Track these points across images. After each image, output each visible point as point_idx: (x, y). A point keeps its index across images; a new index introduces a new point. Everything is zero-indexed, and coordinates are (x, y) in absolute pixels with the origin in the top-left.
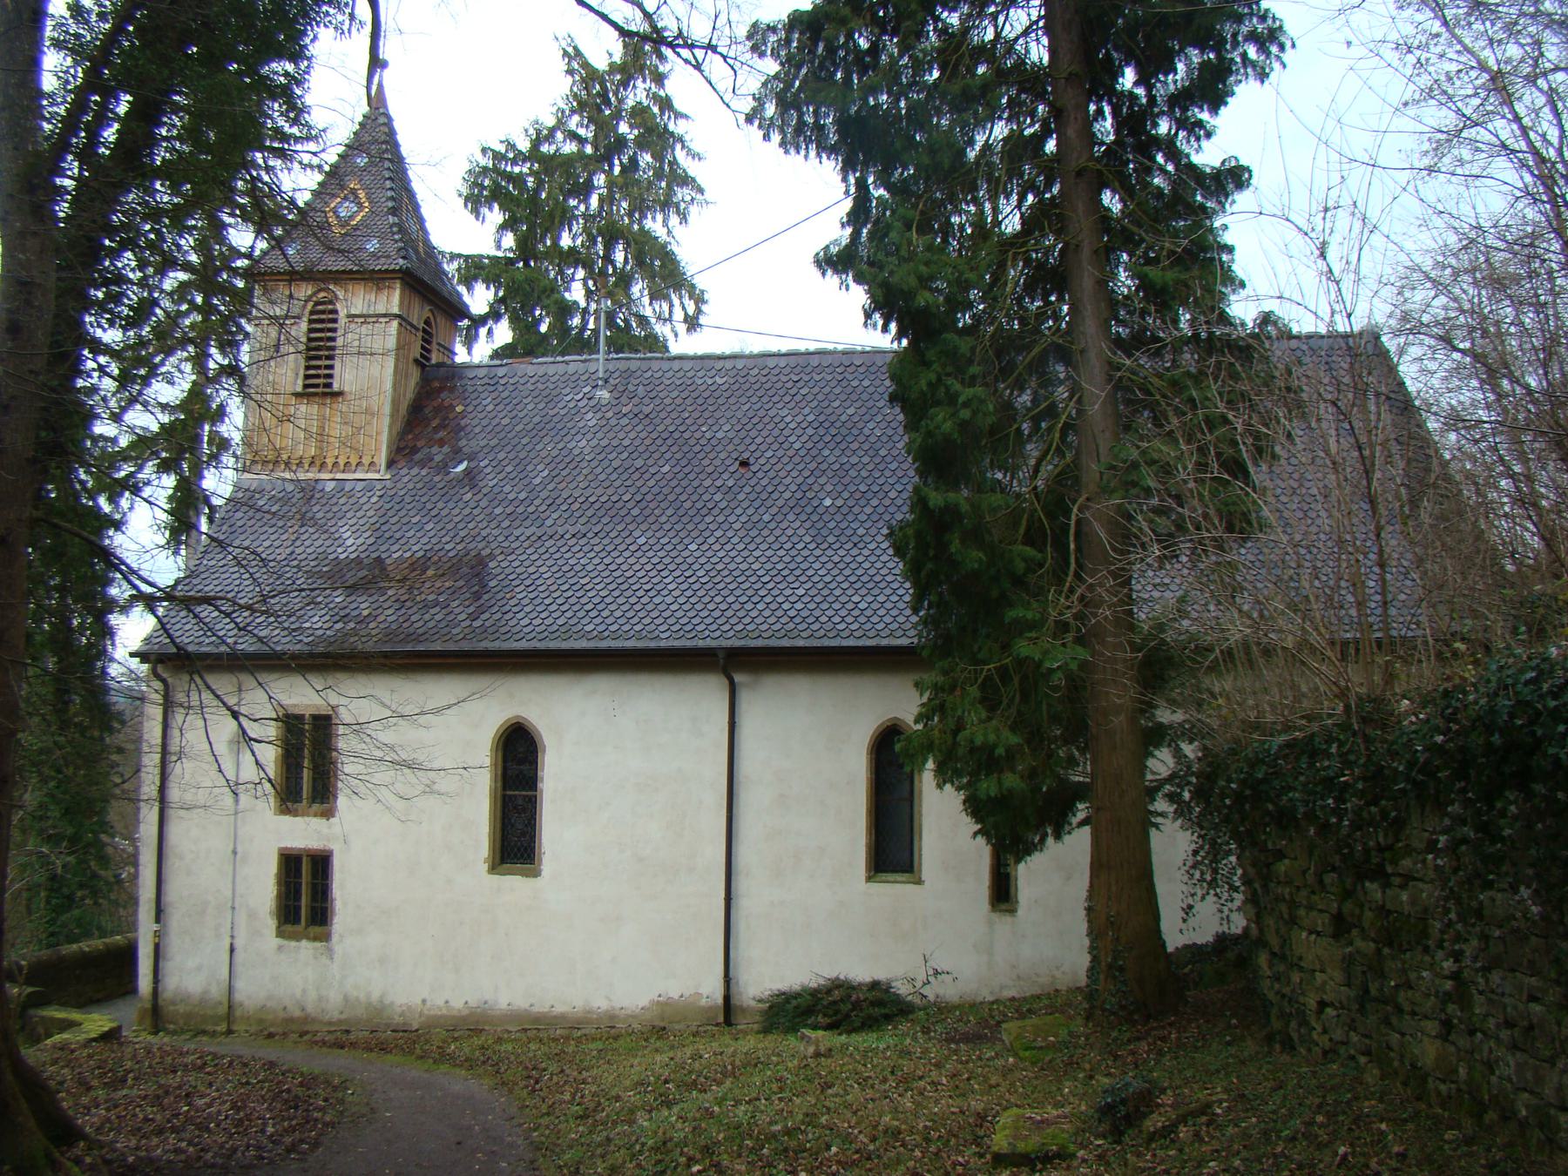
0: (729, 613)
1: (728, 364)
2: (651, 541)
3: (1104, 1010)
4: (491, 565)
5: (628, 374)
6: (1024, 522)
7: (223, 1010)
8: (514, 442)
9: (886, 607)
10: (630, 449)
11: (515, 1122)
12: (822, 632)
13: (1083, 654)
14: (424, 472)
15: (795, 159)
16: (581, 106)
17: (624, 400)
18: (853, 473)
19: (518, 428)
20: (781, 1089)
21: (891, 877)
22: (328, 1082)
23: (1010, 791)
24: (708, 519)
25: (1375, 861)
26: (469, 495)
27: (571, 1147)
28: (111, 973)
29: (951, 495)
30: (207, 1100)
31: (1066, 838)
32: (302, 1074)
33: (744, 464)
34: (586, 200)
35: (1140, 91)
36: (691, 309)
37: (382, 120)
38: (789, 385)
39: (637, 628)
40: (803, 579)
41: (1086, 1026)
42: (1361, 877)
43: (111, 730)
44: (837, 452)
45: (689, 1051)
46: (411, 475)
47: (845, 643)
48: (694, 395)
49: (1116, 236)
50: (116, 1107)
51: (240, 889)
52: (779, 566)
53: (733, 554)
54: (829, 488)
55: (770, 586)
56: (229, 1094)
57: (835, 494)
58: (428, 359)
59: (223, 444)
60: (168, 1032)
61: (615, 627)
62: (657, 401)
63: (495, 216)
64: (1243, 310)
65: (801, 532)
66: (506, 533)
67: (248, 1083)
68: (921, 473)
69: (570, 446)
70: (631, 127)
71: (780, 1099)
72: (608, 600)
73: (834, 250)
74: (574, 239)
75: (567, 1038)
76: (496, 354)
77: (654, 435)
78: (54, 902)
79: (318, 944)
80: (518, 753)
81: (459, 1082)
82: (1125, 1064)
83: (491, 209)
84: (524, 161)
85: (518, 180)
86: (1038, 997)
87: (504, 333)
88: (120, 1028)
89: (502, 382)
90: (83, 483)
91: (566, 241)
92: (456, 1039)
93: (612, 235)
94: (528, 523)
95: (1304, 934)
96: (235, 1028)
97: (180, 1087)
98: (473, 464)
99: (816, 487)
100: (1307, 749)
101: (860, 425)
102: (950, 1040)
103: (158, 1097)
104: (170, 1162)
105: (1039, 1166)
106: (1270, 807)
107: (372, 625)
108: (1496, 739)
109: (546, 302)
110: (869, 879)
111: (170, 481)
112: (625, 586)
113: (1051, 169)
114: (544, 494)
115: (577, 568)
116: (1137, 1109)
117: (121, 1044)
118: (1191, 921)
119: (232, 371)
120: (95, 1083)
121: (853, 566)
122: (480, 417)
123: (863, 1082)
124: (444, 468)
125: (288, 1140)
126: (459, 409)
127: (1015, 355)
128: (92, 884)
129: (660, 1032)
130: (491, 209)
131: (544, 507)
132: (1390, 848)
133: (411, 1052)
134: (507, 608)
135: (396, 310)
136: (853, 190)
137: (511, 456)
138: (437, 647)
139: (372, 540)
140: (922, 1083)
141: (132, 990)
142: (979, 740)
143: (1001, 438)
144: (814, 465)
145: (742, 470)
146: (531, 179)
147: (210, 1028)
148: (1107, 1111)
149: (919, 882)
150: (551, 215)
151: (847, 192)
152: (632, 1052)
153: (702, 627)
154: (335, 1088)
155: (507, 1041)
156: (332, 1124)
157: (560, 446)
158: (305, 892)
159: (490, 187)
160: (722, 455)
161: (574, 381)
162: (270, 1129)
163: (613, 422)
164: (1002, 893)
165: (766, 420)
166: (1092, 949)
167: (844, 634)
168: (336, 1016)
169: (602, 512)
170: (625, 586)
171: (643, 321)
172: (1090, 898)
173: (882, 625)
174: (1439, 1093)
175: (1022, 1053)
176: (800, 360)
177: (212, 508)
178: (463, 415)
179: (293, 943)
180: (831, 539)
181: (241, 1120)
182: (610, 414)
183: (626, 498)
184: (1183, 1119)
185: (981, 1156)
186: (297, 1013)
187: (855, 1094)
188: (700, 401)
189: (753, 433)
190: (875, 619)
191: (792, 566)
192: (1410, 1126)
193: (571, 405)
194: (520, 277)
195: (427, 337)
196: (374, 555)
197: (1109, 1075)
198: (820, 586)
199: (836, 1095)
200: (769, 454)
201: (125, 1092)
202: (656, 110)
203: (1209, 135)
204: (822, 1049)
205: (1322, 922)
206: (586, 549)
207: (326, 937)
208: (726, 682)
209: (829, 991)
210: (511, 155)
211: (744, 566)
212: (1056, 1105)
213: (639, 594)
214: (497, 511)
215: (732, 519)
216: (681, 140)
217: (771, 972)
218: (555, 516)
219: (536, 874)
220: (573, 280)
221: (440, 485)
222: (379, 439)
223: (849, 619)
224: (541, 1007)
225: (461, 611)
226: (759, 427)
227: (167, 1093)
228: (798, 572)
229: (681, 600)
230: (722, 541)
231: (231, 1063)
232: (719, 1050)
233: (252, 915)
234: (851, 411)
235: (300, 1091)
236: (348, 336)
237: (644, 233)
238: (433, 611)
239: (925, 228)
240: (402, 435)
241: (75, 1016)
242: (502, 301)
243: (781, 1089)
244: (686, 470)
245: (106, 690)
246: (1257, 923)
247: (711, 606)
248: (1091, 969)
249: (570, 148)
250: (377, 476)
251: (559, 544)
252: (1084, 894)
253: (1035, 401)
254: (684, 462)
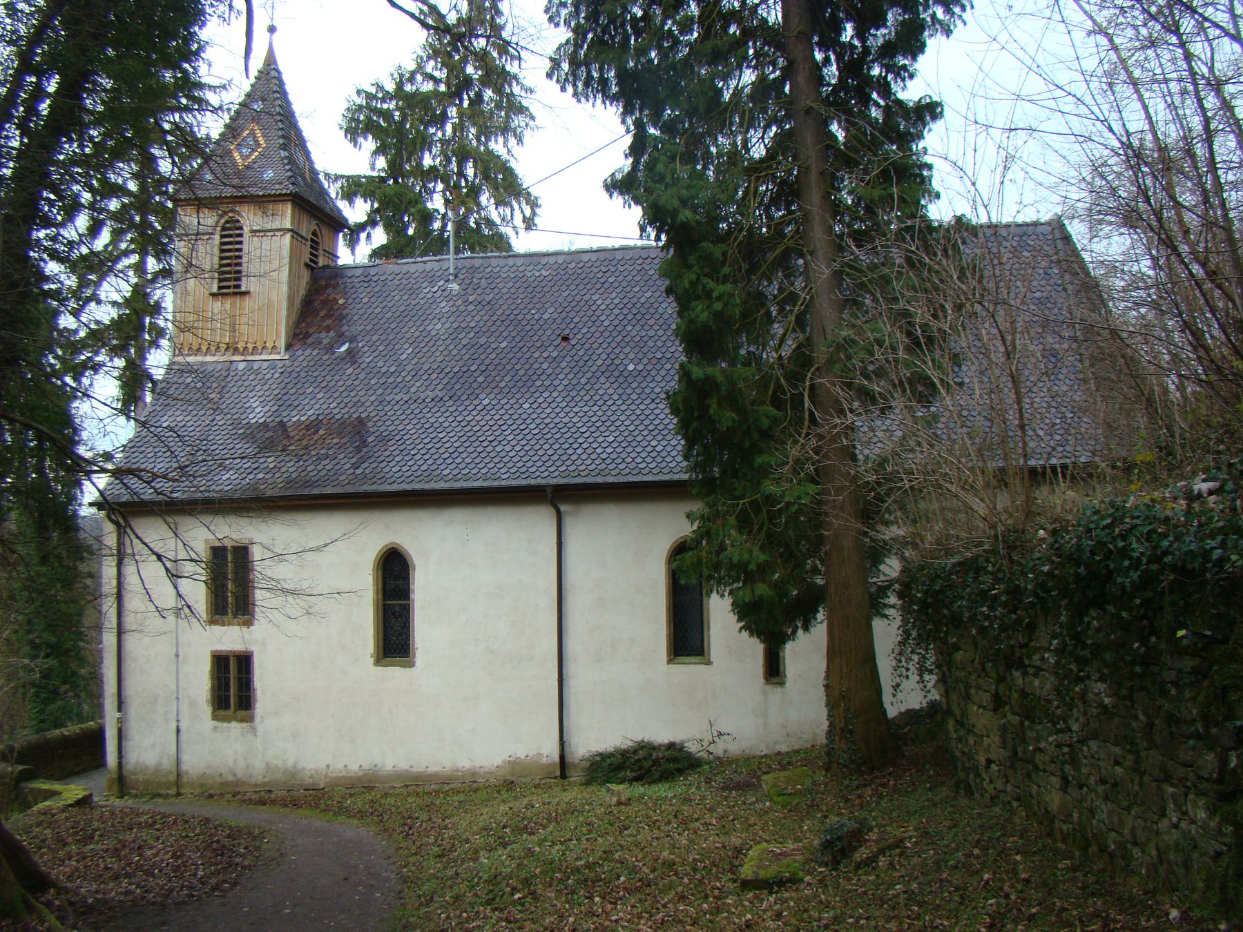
0: (555, 457)
1: (552, 260)
2: (494, 402)
3: (839, 764)
4: (370, 424)
5: (473, 270)
6: (772, 386)
7: (173, 777)
8: (385, 327)
9: (667, 456)
10: (477, 329)
11: (391, 861)
12: (628, 470)
13: (812, 489)
14: (315, 353)
15: (586, 106)
16: (435, 54)
17: (470, 291)
18: (650, 344)
19: (387, 316)
20: (590, 831)
21: (686, 659)
22: (250, 833)
23: (761, 598)
24: (538, 383)
25: (1018, 654)
26: (351, 370)
27: (428, 880)
28: (86, 751)
29: (709, 370)
30: (154, 851)
31: (812, 630)
32: (230, 828)
33: (565, 339)
34: (442, 127)
35: (856, 42)
36: (528, 212)
37: (274, 74)
38: (599, 275)
39: (484, 471)
40: (612, 428)
41: (826, 776)
42: (1009, 666)
43: (82, 559)
44: (638, 327)
45: (525, 801)
46: (305, 355)
47: (645, 479)
48: (525, 285)
49: (846, 159)
50: (84, 858)
51: (182, 683)
52: (594, 419)
53: (558, 410)
54: (632, 356)
55: (586, 435)
56: (172, 846)
57: (636, 361)
58: (316, 263)
59: (161, 333)
60: (131, 796)
61: (466, 471)
62: (496, 291)
63: (369, 144)
64: (939, 212)
65: (611, 391)
66: (380, 399)
67: (187, 836)
68: (688, 352)
69: (428, 328)
70: (476, 68)
71: (588, 840)
72: (460, 450)
73: (619, 176)
74: (433, 159)
75: (437, 792)
76: (376, 254)
77: (495, 318)
78: (43, 696)
79: (244, 725)
80: (394, 571)
81: (352, 830)
82: (853, 806)
83: (366, 139)
84: (391, 100)
85: (387, 115)
86: (798, 752)
87: (380, 237)
88: (91, 795)
89: (375, 279)
90: (52, 366)
91: (427, 161)
92: (351, 795)
93: (464, 155)
94: (397, 390)
95: (975, 708)
96: (182, 791)
97: (134, 841)
98: (353, 345)
99: (622, 356)
100: (971, 567)
101: (655, 306)
102: (723, 789)
103: (117, 850)
104: (120, 901)
105: (776, 889)
106: (945, 612)
107: (277, 475)
108: (1082, 570)
109: (413, 210)
110: (670, 661)
111: (120, 363)
112: (474, 438)
113: (790, 104)
114: (409, 367)
115: (436, 425)
116: (850, 843)
117: (92, 808)
118: (900, 696)
119: (166, 273)
120: (70, 840)
121: (651, 417)
122: (360, 309)
123: (653, 824)
124: (330, 348)
125: (213, 881)
126: (341, 301)
127: (757, 254)
128: (70, 678)
129: (509, 785)
130: (366, 139)
131: (409, 378)
132: (1026, 645)
133: (317, 807)
134: (382, 458)
135: (288, 226)
136: (632, 128)
137: (383, 338)
138: (329, 490)
139: (276, 408)
140: (697, 824)
141: (100, 762)
142: (736, 559)
143: (753, 317)
144: (620, 337)
145: (564, 344)
146: (397, 113)
147: (163, 792)
148: (827, 845)
149: (709, 663)
150: (414, 142)
151: (628, 131)
152: (485, 802)
153: (534, 469)
154: (255, 838)
155: (391, 795)
156: (249, 867)
157: (421, 328)
158: (233, 685)
159: (363, 121)
160: (548, 333)
161: (431, 278)
162: (200, 873)
163: (462, 308)
164: (774, 670)
165: (582, 303)
166: (829, 716)
167: (644, 472)
168: (260, 780)
169: (455, 380)
170: (474, 438)
171: (490, 223)
172: (827, 677)
173: (674, 464)
174: (1062, 832)
175: (775, 799)
176: (608, 255)
177: (154, 382)
178: (344, 306)
179: (225, 725)
180: (634, 397)
181: (178, 866)
182: (460, 302)
183: (473, 368)
184: (882, 852)
185: (735, 881)
186: (231, 778)
187: (646, 834)
188: (530, 290)
189: (572, 314)
190: (669, 459)
191: (604, 419)
192: (1037, 858)
193: (429, 296)
194: (390, 192)
195: (315, 245)
196: (278, 420)
197: (840, 814)
198: (626, 434)
199: (630, 836)
200: (584, 331)
201: (92, 846)
202: (495, 54)
203: (911, 77)
204: (623, 799)
205: (986, 698)
206: (443, 410)
207: (250, 719)
208: (554, 511)
209: (635, 752)
210: (380, 95)
211: (566, 420)
212: (796, 840)
213: (485, 444)
214: (373, 382)
215: (557, 382)
216: (515, 77)
217: (597, 735)
218: (418, 384)
219: (411, 665)
220: (434, 191)
221: (328, 363)
222: (279, 331)
223: (649, 460)
224: (418, 768)
225: (346, 462)
226: (577, 309)
227: (124, 846)
228: (608, 424)
229: (518, 448)
230: (549, 400)
231: (175, 821)
232: (547, 801)
233: (193, 703)
234: (648, 294)
235: (226, 842)
236: (251, 246)
237: (490, 153)
238: (324, 463)
239: (689, 158)
240: (297, 324)
241: (57, 786)
242: (377, 211)
243: (590, 831)
244: (520, 345)
245: (78, 529)
246: (947, 698)
247: (541, 453)
248: (829, 732)
249: (428, 87)
250: (278, 357)
251: (422, 406)
252: (824, 674)
253: (780, 290)
254: (518, 339)
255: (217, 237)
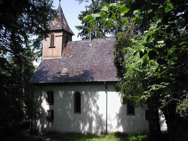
110: (127, 115)
163: (92, 49)
255: (50, 37)
